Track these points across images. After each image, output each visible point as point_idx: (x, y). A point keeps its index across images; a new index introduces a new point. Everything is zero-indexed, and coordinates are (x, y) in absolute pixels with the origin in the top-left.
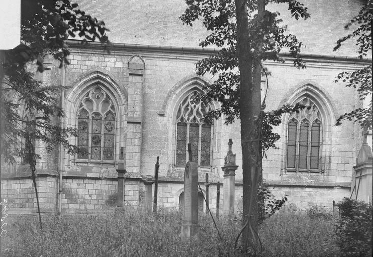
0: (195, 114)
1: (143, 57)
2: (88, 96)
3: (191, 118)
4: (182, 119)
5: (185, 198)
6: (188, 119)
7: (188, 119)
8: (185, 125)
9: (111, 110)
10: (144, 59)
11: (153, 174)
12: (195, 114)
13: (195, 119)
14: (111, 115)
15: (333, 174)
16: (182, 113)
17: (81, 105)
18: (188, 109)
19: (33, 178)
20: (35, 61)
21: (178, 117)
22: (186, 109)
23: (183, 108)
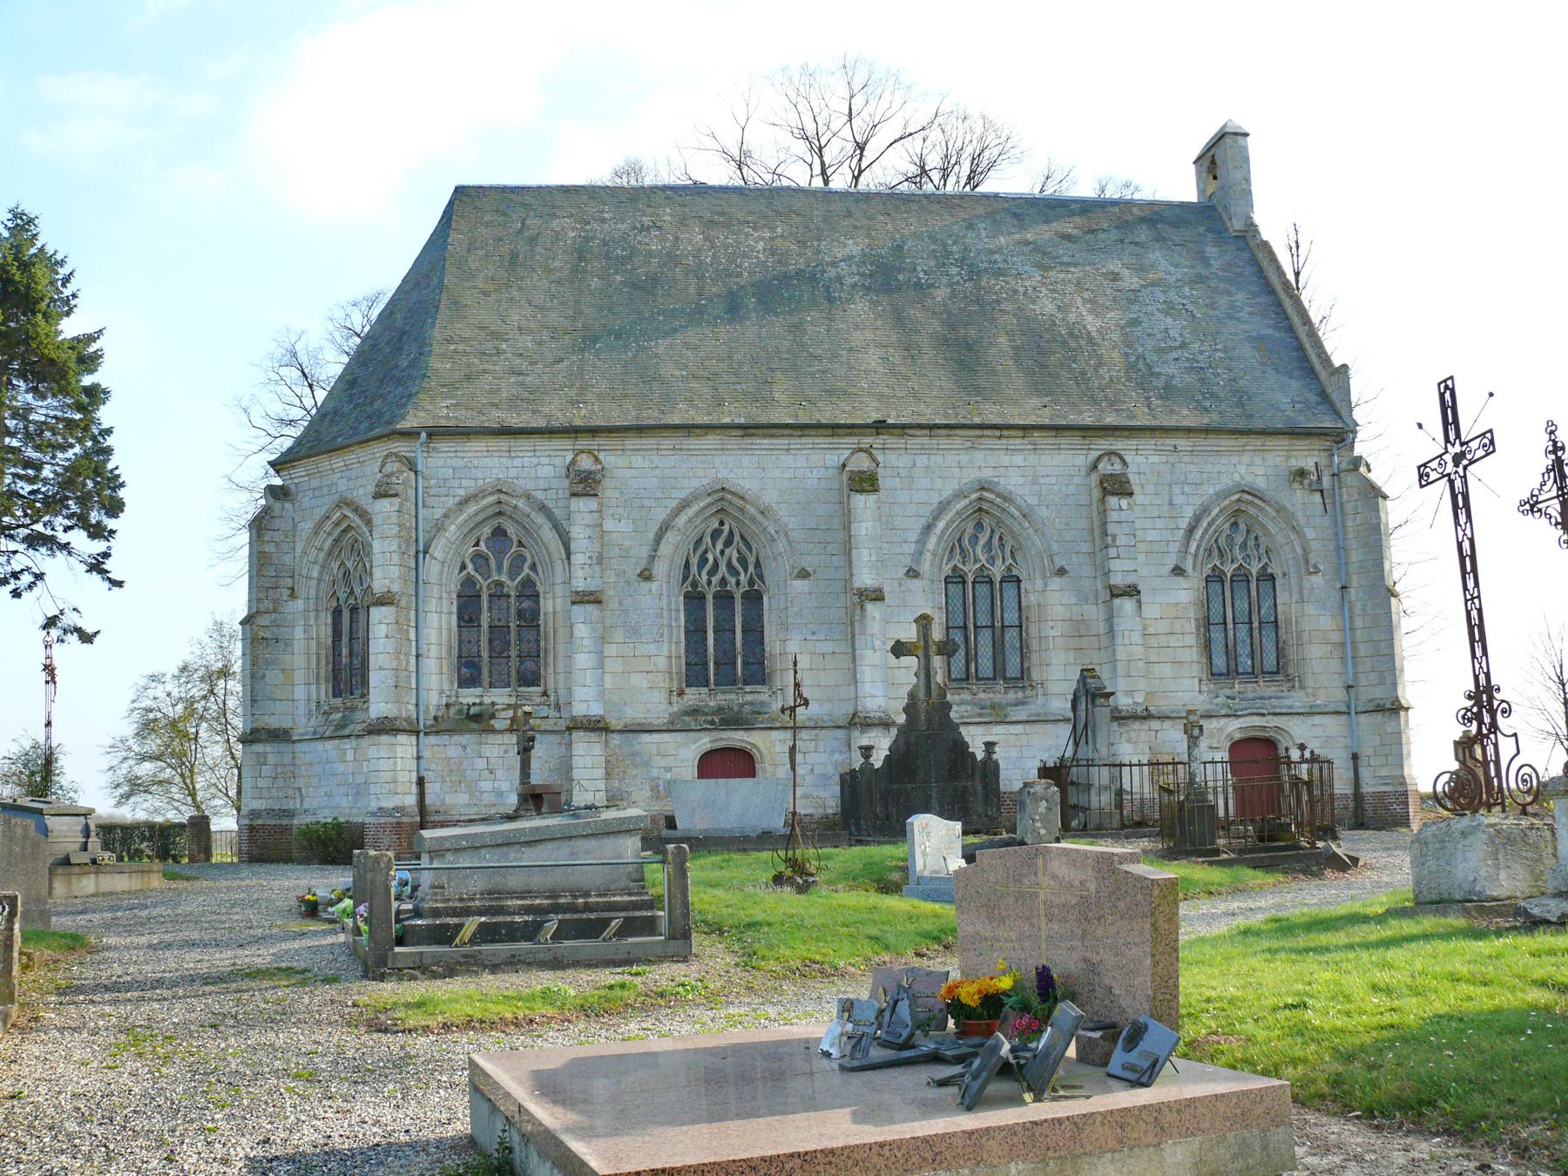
0: (723, 569)
1: (599, 450)
2: (477, 544)
3: (715, 580)
4: (695, 584)
5: (1467, 954)
6: (709, 583)
7: (709, 583)
8: (702, 597)
9: (531, 573)
10: (602, 456)
11: (411, 800)
12: (723, 569)
13: (723, 581)
14: (529, 591)
15: (426, 753)
16: (694, 569)
17: (463, 567)
18: (707, 560)
19: (794, 728)
20: (835, 1052)
21: (685, 578)
22: (703, 561)
23: (694, 561)
